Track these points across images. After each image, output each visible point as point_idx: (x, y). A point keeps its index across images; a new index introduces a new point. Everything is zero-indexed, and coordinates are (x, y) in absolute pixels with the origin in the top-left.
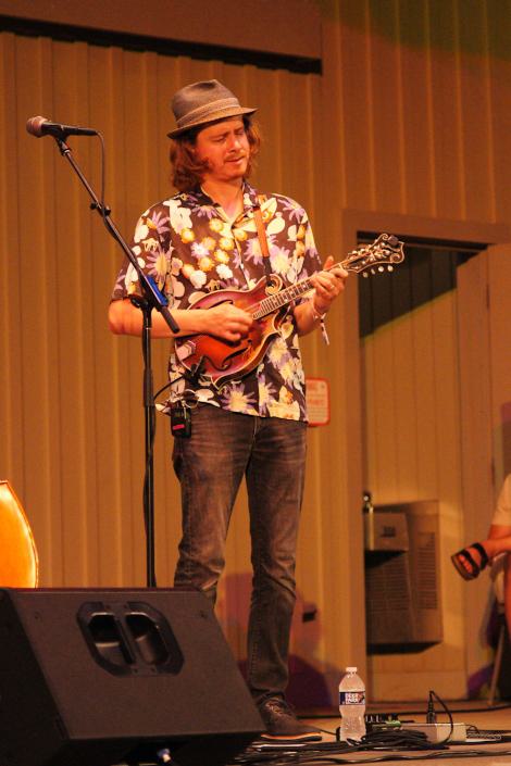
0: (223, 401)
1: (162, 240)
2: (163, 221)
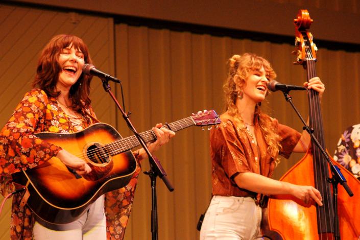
0: (340, 156)
1: (347, 145)
2: (348, 136)
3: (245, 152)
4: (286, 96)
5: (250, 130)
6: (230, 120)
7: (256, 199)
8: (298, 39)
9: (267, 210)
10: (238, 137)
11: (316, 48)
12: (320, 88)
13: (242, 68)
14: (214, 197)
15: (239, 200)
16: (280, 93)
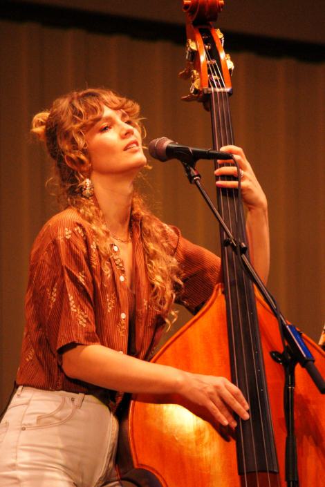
3: (94, 300)
4: (188, 171)
6: (80, 225)
8: (193, 46)
10: (89, 264)
11: (230, 65)
14: (20, 388)
15: (73, 400)
16: (176, 164)
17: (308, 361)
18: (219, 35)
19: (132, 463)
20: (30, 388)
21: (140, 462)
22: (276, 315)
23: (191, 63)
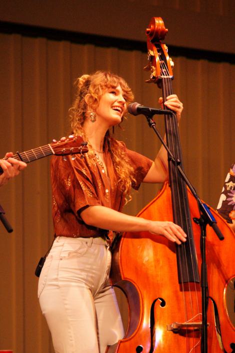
3: (93, 182)
4: (149, 121)
5: (100, 158)
7: (108, 238)
8: (152, 53)
9: (118, 255)
10: (87, 165)
11: (172, 64)
12: (179, 107)
13: (95, 86)
14: (58, 238)
15: (87, 243)
16: (142, 117)
17: (213, 223)
18: (165, 47)
19: (121, 277)
20: (62, 237)
21: (125, 277)
22: (196, 198)
23: (151, 62)
